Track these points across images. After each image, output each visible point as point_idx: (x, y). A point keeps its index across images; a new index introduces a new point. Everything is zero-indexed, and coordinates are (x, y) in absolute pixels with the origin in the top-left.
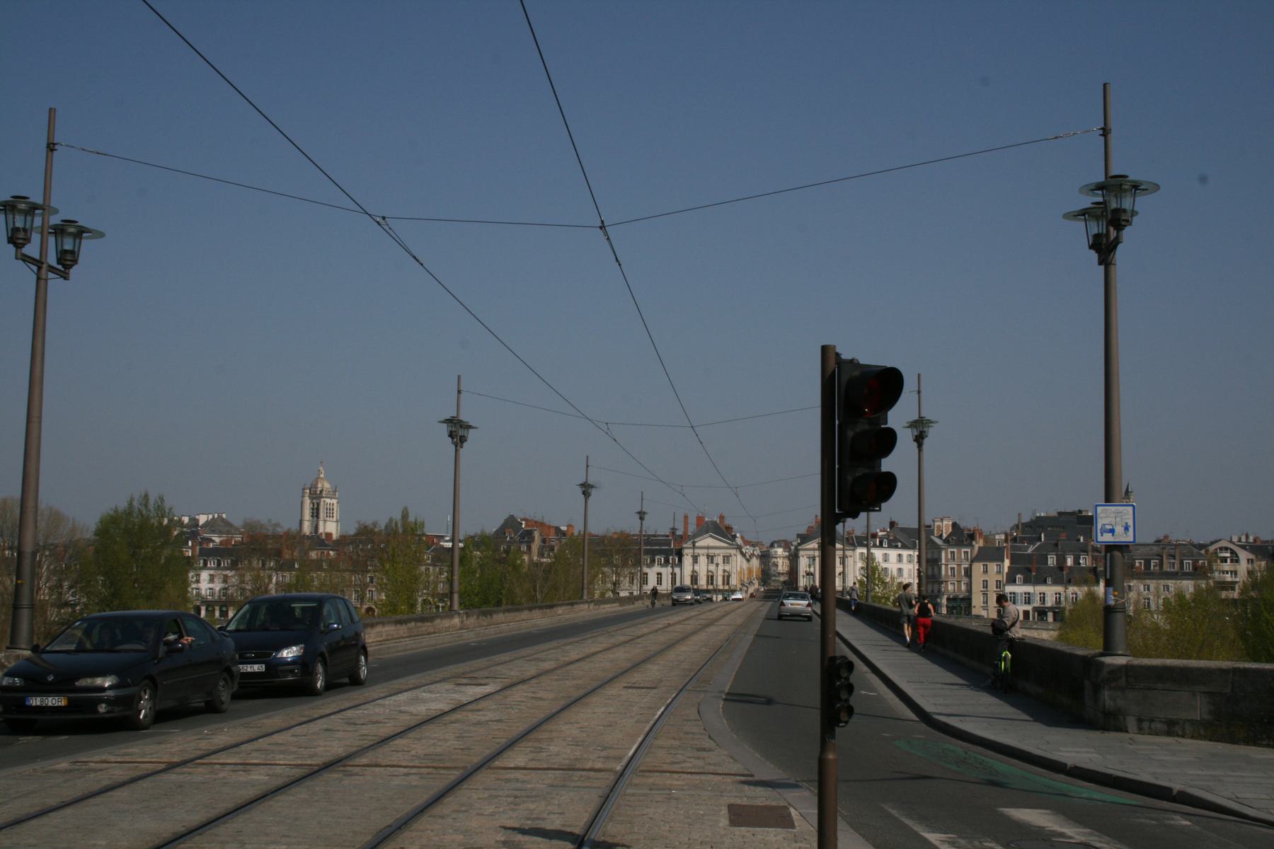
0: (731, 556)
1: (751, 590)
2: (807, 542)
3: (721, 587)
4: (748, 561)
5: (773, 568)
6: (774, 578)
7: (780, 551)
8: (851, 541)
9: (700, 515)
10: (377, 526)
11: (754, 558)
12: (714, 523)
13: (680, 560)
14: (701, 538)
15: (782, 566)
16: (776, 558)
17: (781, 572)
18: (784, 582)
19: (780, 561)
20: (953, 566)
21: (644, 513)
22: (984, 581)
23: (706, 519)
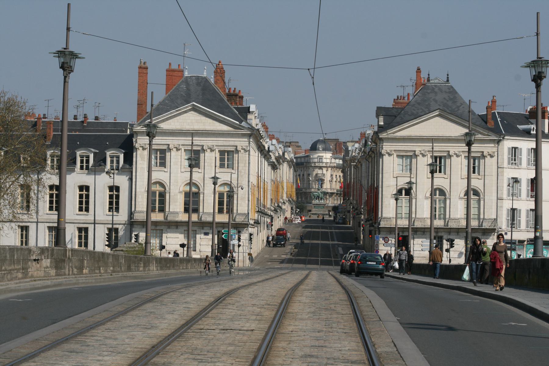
0: (237, 151)
1: (278, 223)
2: (399, 124)
3: (184, 217)
4: (274, 167)
5: (315, 186)
6: (317, 202)
7: (327, 157)
8: (491, 124)
9: (174, 67)
11: (285, 165)
12: (202, 82)
13: (129, 160)
14: (174, 112)
15: (331, 181)
16: (321, 168)
17: (329, 191)
18: (335, 209)
19: (327, 174)
21: (74, 55)
23: (186, 74)
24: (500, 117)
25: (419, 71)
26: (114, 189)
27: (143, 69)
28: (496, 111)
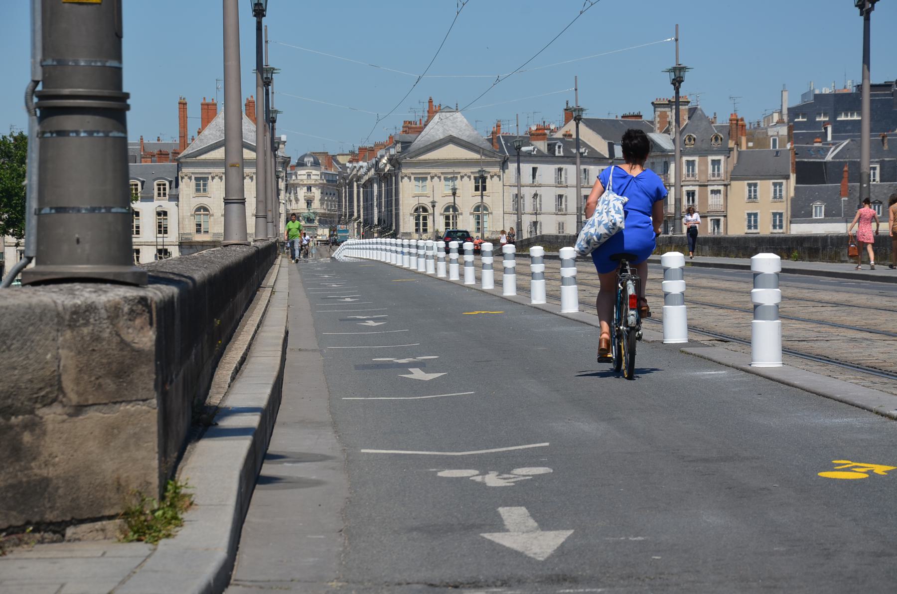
9: (209, 101)
10: (177, 529)
20: (691, 188)
22: (749, 215)
24: (504, 140)
25: (430, 101)
26: (162, 214)
27: (183, 105)
28: (500, 135)
